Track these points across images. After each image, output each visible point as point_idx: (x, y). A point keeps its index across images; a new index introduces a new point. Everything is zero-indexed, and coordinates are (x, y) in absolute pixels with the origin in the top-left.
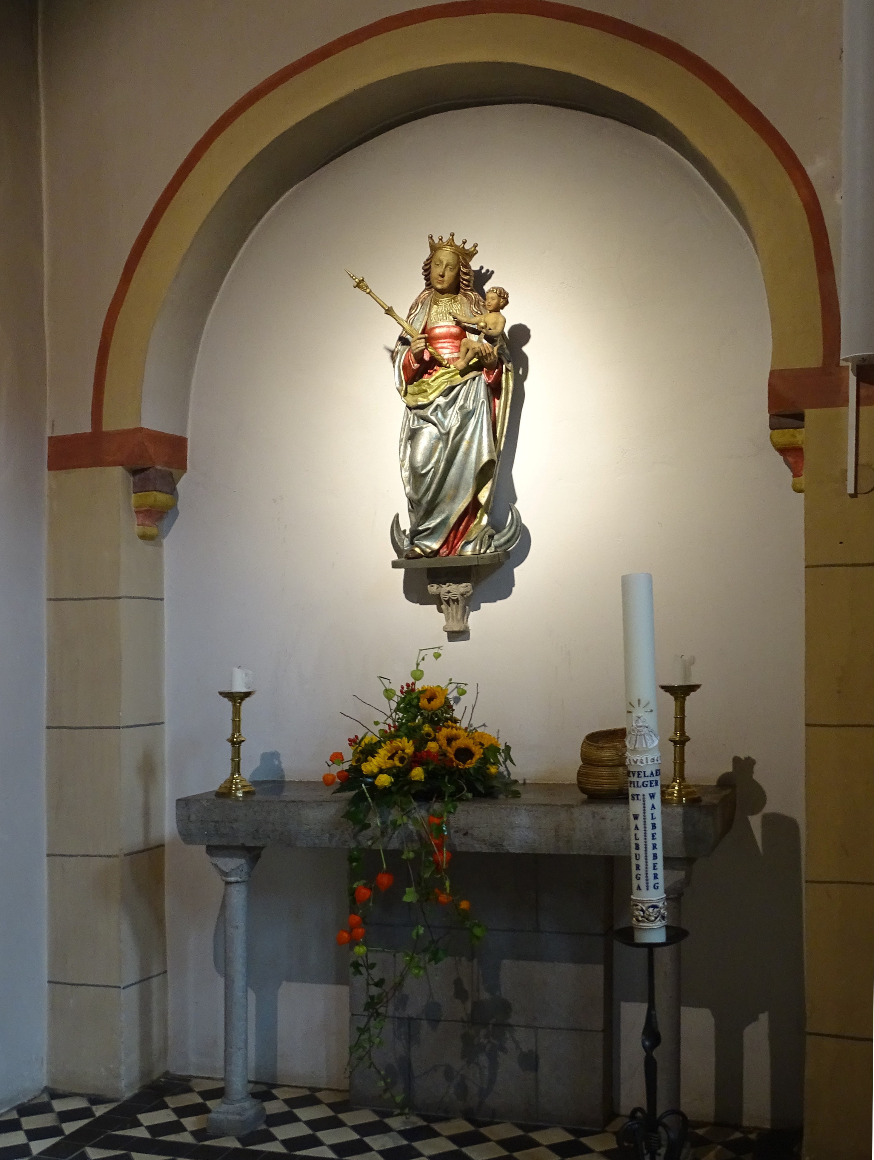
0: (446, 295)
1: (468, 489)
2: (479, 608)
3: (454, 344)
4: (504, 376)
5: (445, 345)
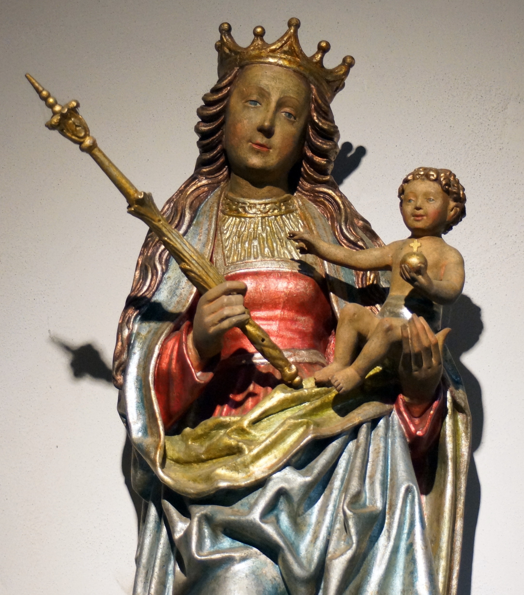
0: (266, 189)
3: (294, 327)
4: (448, 421)
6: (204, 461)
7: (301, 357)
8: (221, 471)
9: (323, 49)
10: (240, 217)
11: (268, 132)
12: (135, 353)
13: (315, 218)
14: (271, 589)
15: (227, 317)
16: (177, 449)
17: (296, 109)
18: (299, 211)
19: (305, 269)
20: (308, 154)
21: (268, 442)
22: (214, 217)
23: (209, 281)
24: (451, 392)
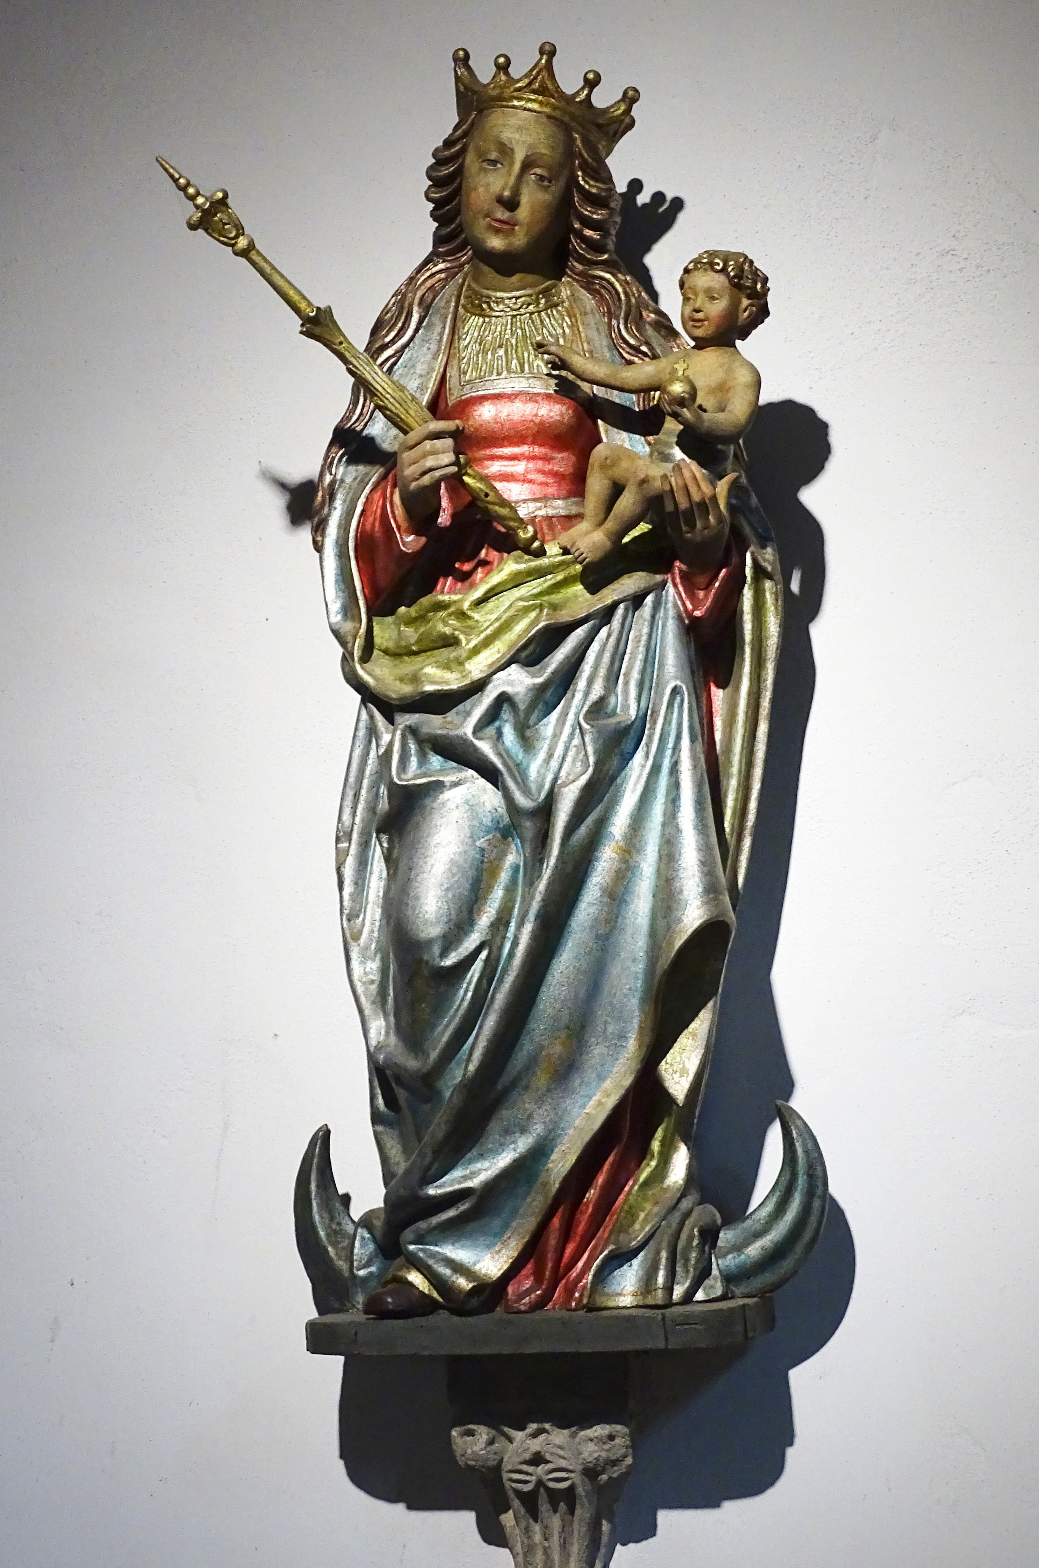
0: (515, 278)
1: (622, 1037)
2: (649, 1530)
3: (548, 467)
4: (748, 594)
5: (519, 467)
6: (416, 653)
7: (555, 508)
8: (430, 670)
9: (592, 83)
10: (484, 316)
11: (511, 204)
12: (335, 508)
13: (586, 314)
14: (489, 824)
15: (431, 470)
16: (387, 636)
17: (550, 168)
18: (566, 304)
19: (566, 389)
20: (576, 226)
21: (488, 632)
22: (450, 317)
23: (410, 420)
24: (752, 554)
